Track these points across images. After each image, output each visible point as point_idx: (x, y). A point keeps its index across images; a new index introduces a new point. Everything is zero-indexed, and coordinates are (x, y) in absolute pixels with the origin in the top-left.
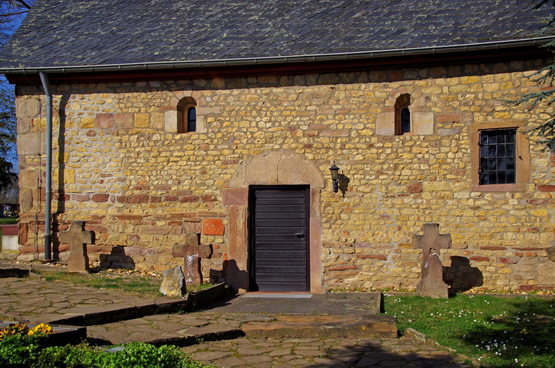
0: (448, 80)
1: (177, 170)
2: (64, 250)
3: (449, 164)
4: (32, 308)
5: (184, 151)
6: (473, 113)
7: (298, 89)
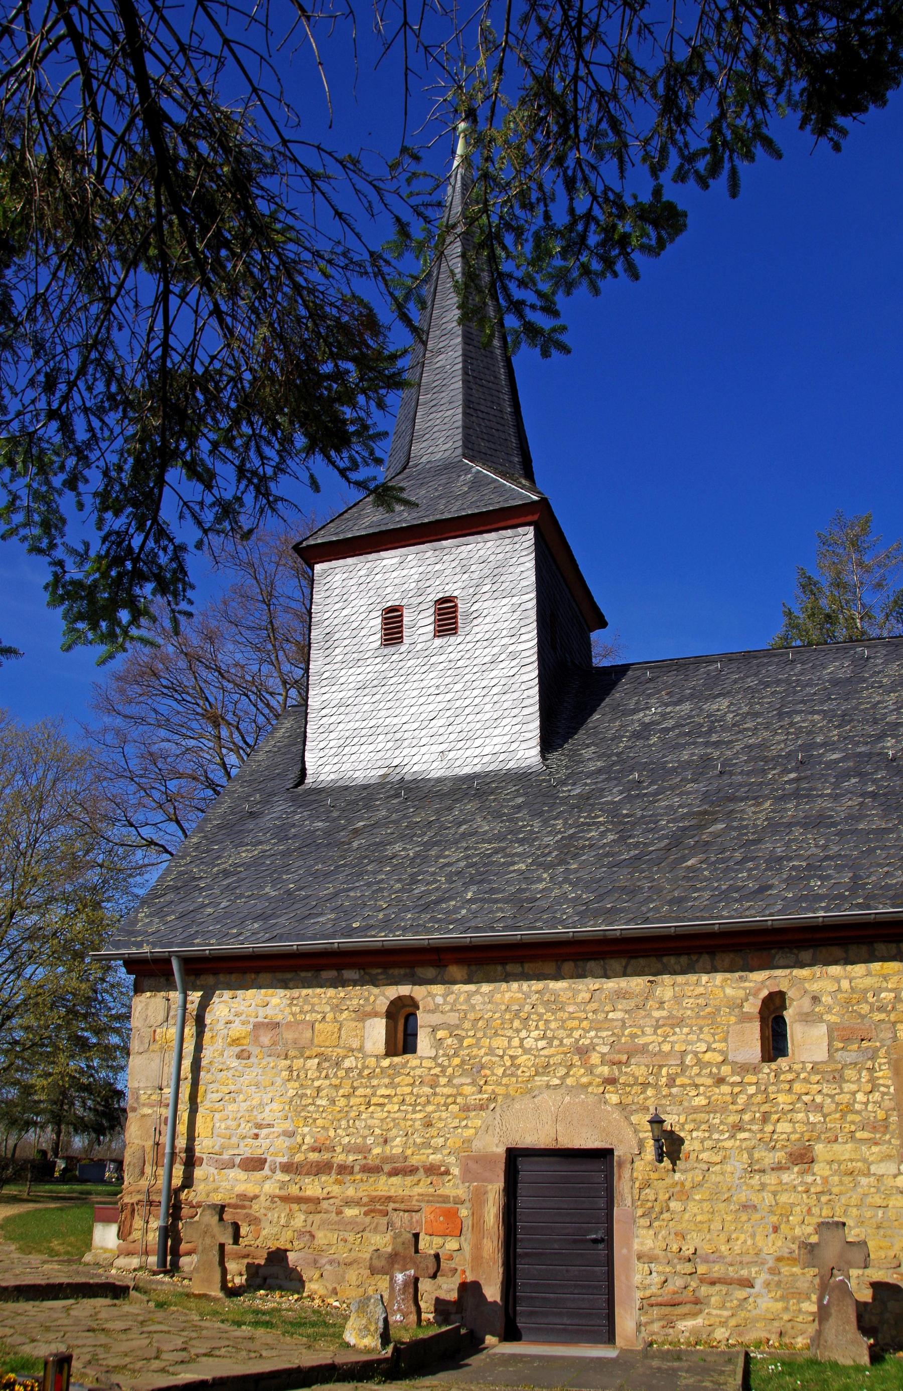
0: (849, 968)
1: (382, 1120)
2: (189, 1253)
3: (858, 1112)
4: (128, 1360)
5: (395, 1088)
6: (894, 1024)
7: (592, 984)
